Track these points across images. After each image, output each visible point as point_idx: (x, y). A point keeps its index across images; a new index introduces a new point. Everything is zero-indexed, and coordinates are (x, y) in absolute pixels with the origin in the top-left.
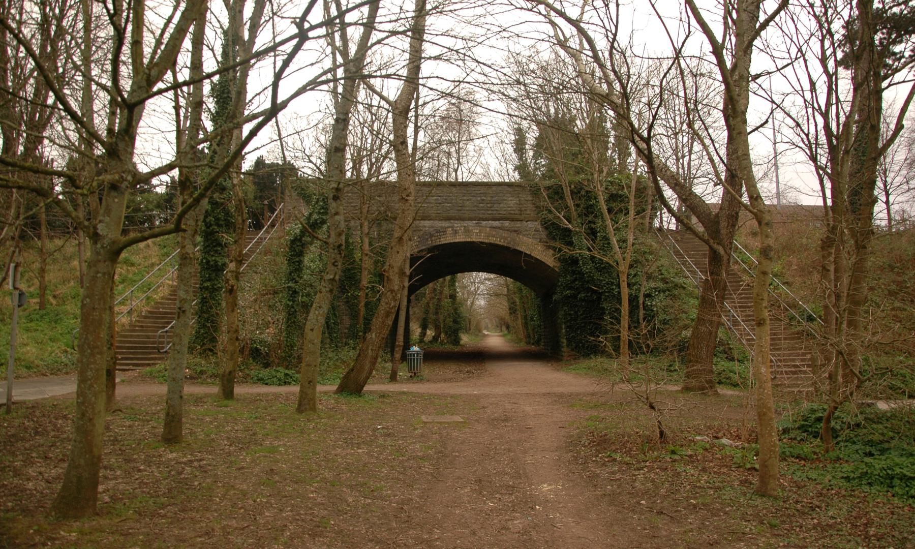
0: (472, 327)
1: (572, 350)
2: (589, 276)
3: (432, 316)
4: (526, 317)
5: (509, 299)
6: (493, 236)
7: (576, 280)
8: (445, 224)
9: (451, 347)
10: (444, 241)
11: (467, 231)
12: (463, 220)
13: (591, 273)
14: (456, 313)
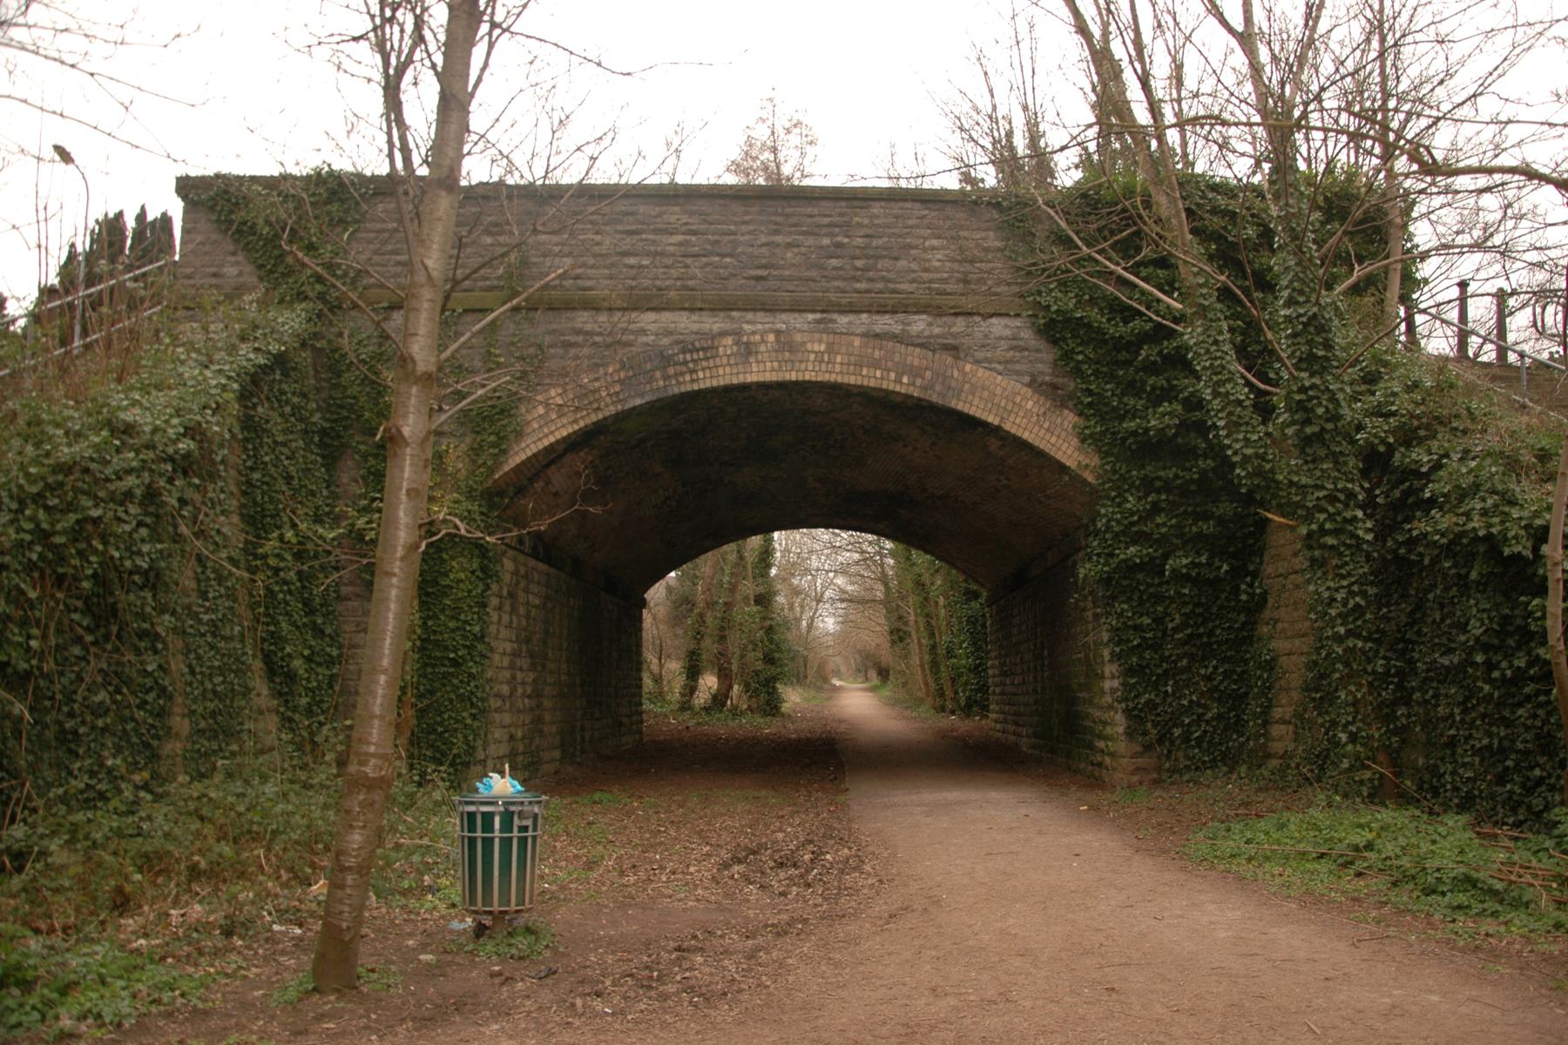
0: (811, 672)
1: (1148, 748)
2: (1259, 472)
3: (709, 646)
4: (933, 647)
5: (888, 612)
6: (875, 365)
7: (1156, 509)
8: (713, 323)
9: (759, 720)
10: (707, 379)
11: (787, 346)
12: (771, 308)
13: (1263, 458)
14: (771, 641)
